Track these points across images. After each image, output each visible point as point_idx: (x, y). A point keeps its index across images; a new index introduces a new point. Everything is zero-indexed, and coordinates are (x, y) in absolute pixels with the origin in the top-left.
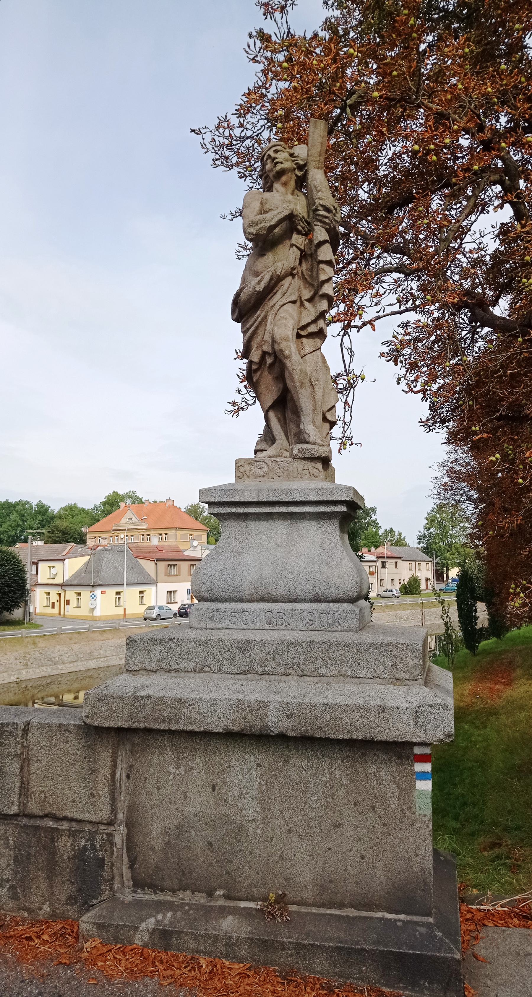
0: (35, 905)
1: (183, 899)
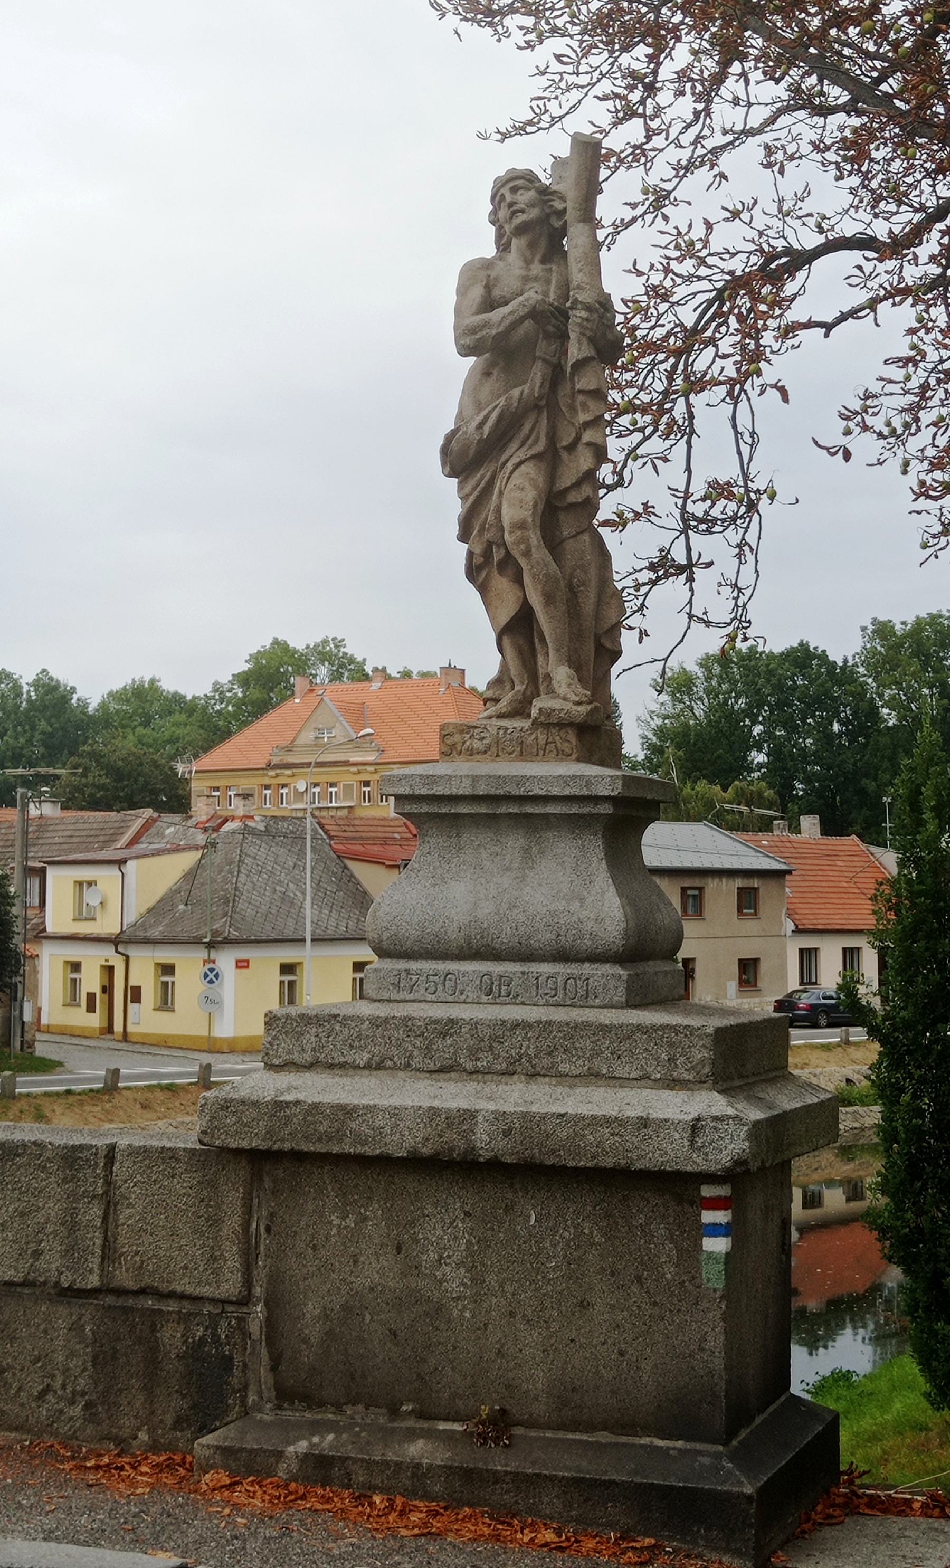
0: (126, 1432)
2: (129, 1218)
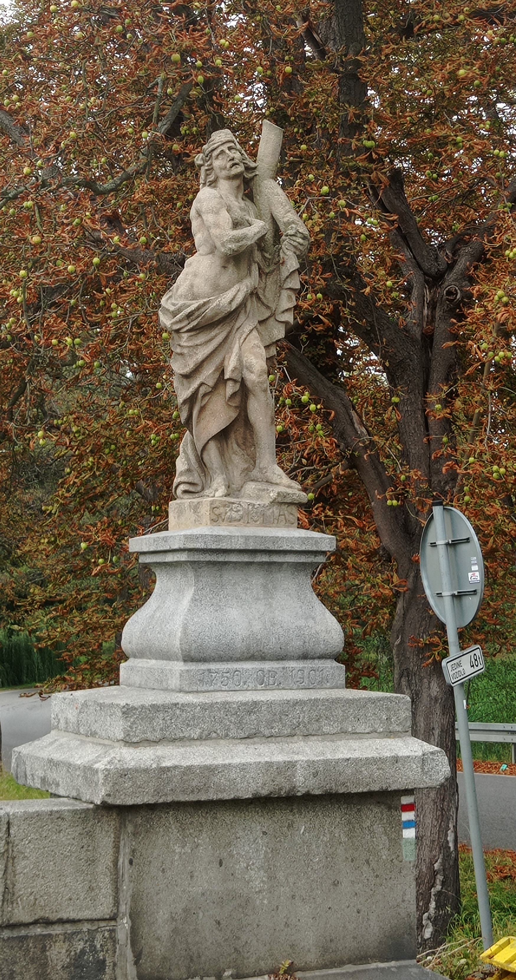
2: (25, 867)
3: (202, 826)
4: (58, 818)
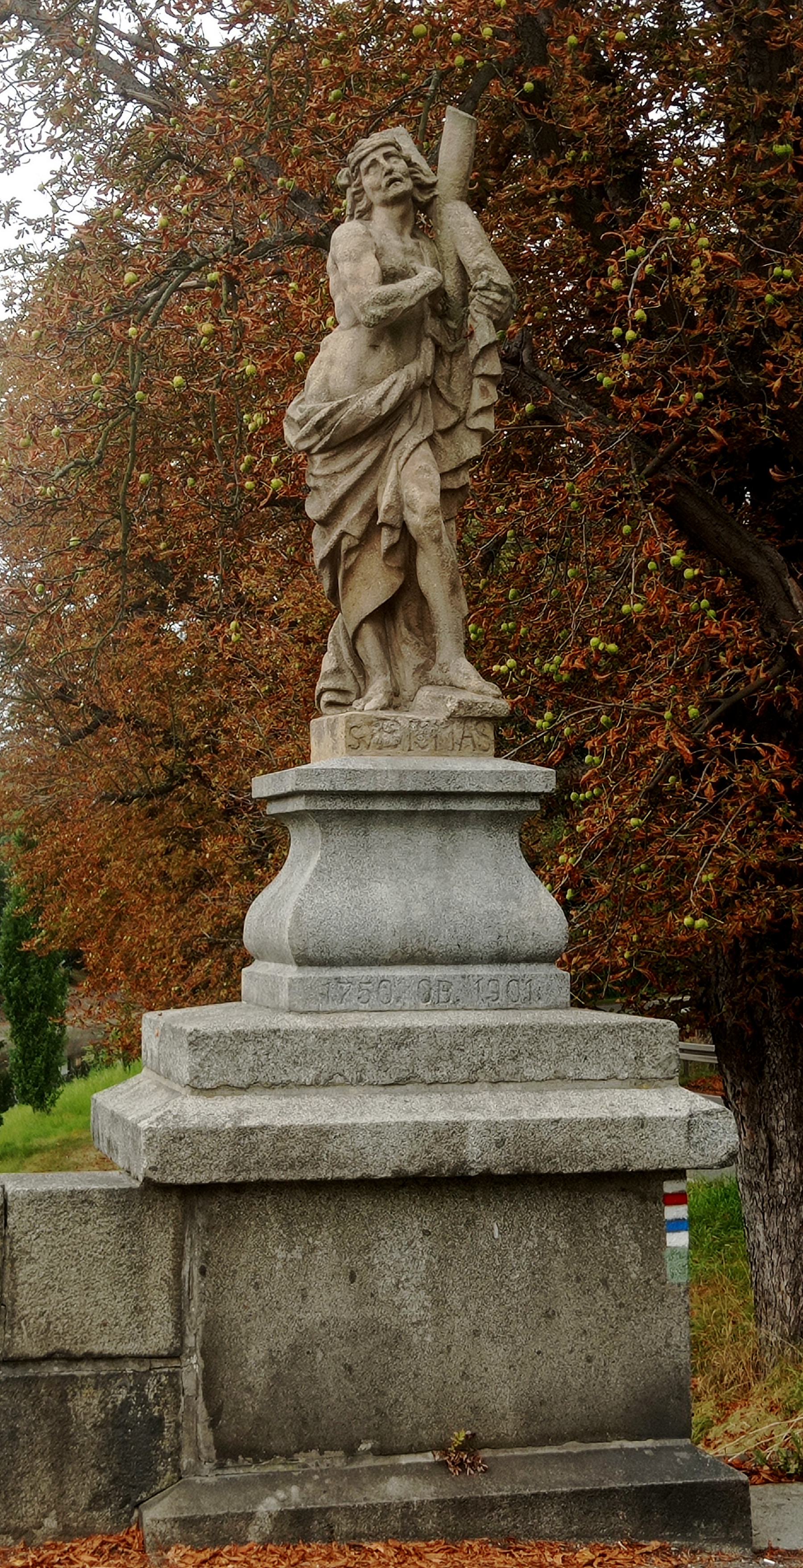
1: (305, 1466)
2: (31, 1275)
3: (321, 1219)
4: (83, 1202)
